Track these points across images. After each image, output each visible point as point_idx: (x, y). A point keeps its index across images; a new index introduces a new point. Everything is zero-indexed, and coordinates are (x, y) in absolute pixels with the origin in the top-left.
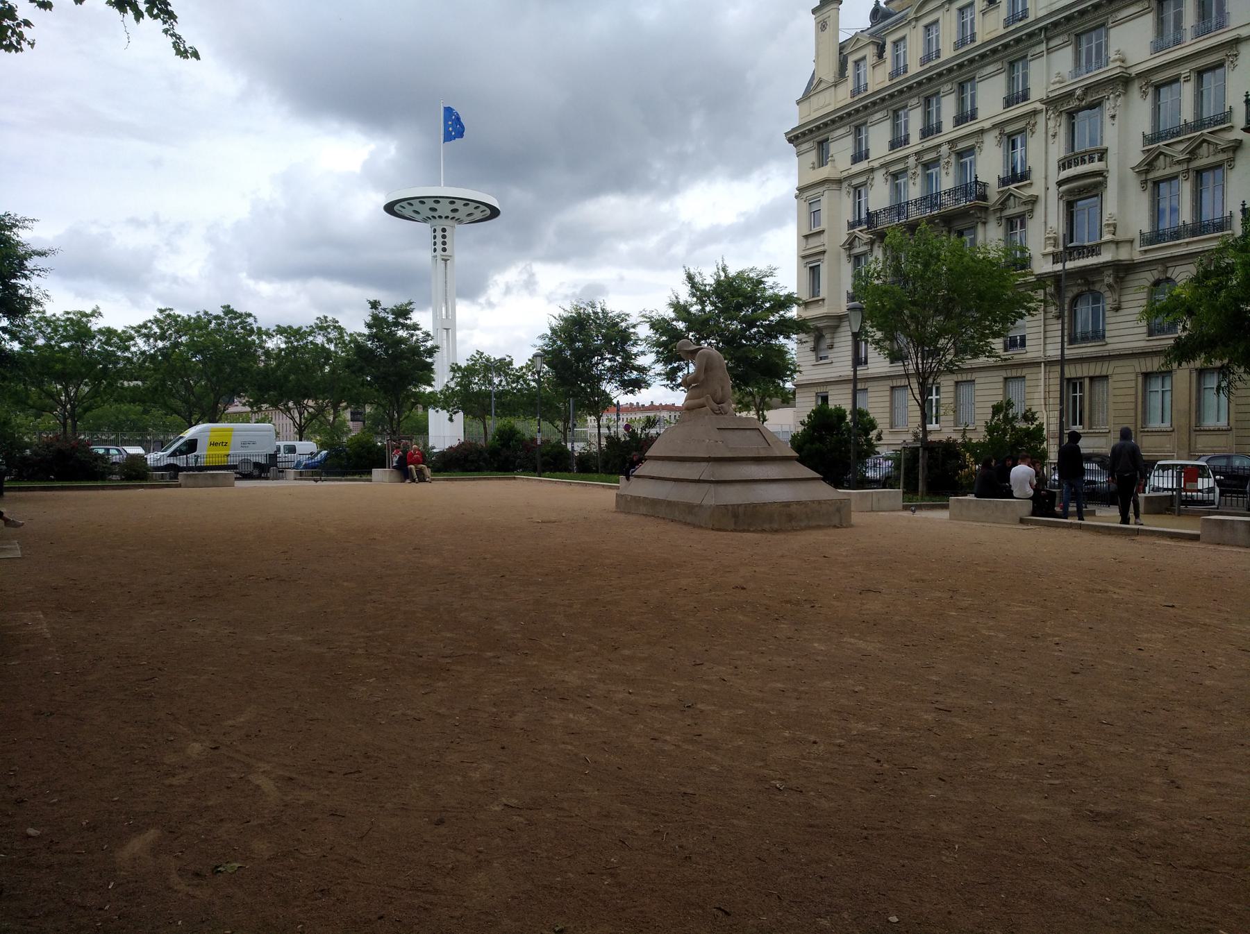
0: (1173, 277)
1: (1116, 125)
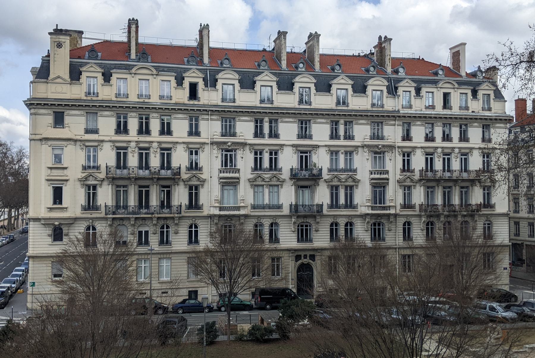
0: (278, 222)
1: (243, 161)
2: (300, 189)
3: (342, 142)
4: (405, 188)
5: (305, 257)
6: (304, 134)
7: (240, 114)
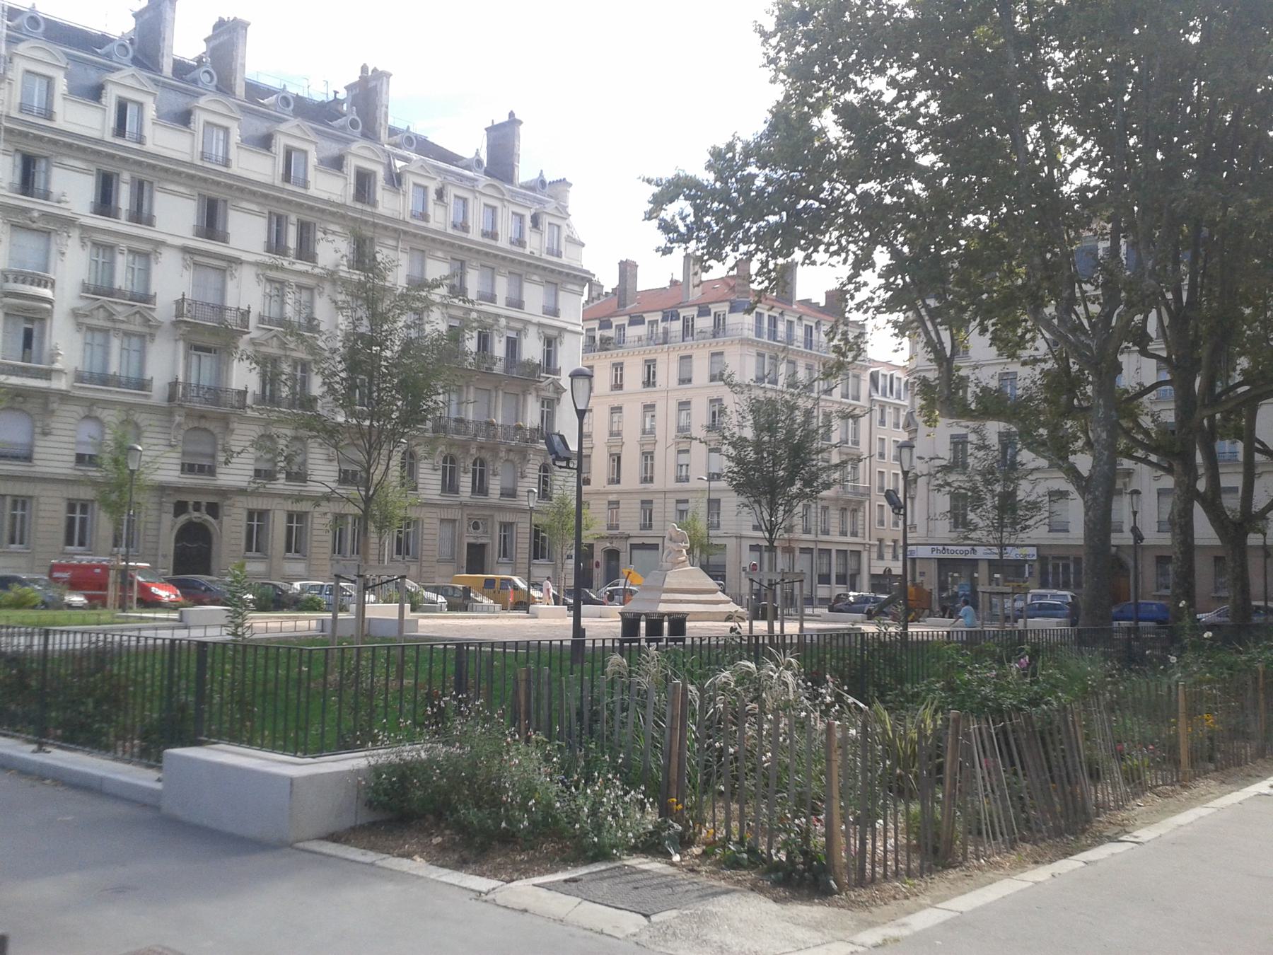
2: (193, 352)
3: (122, 225)
4: (543, 402)
5: (197, 506)
6: (211, 224)
7: (63, 150)
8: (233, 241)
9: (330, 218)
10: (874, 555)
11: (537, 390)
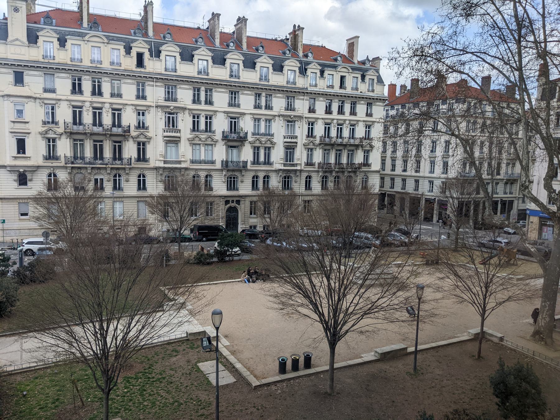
6: (171, 96)
7: (180, 82)
8: (216, 104)
9: (278, 92)
10: (521, 201)
11: (362, 147)
